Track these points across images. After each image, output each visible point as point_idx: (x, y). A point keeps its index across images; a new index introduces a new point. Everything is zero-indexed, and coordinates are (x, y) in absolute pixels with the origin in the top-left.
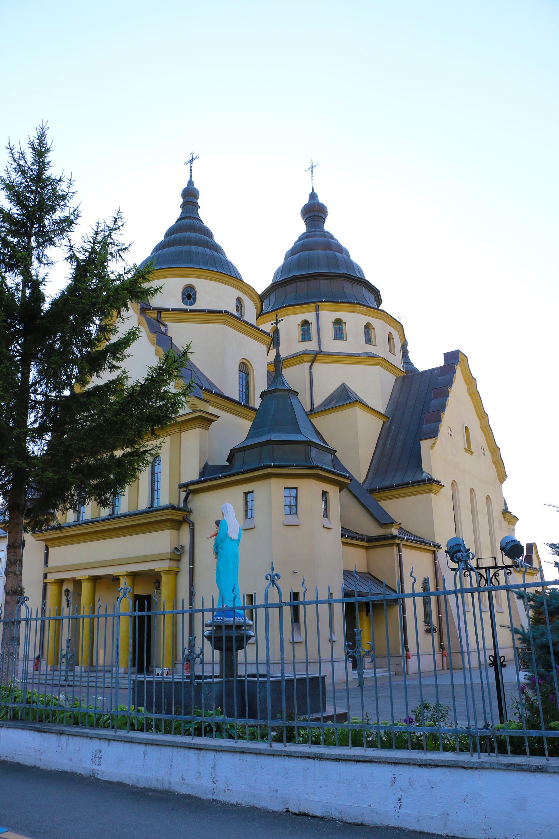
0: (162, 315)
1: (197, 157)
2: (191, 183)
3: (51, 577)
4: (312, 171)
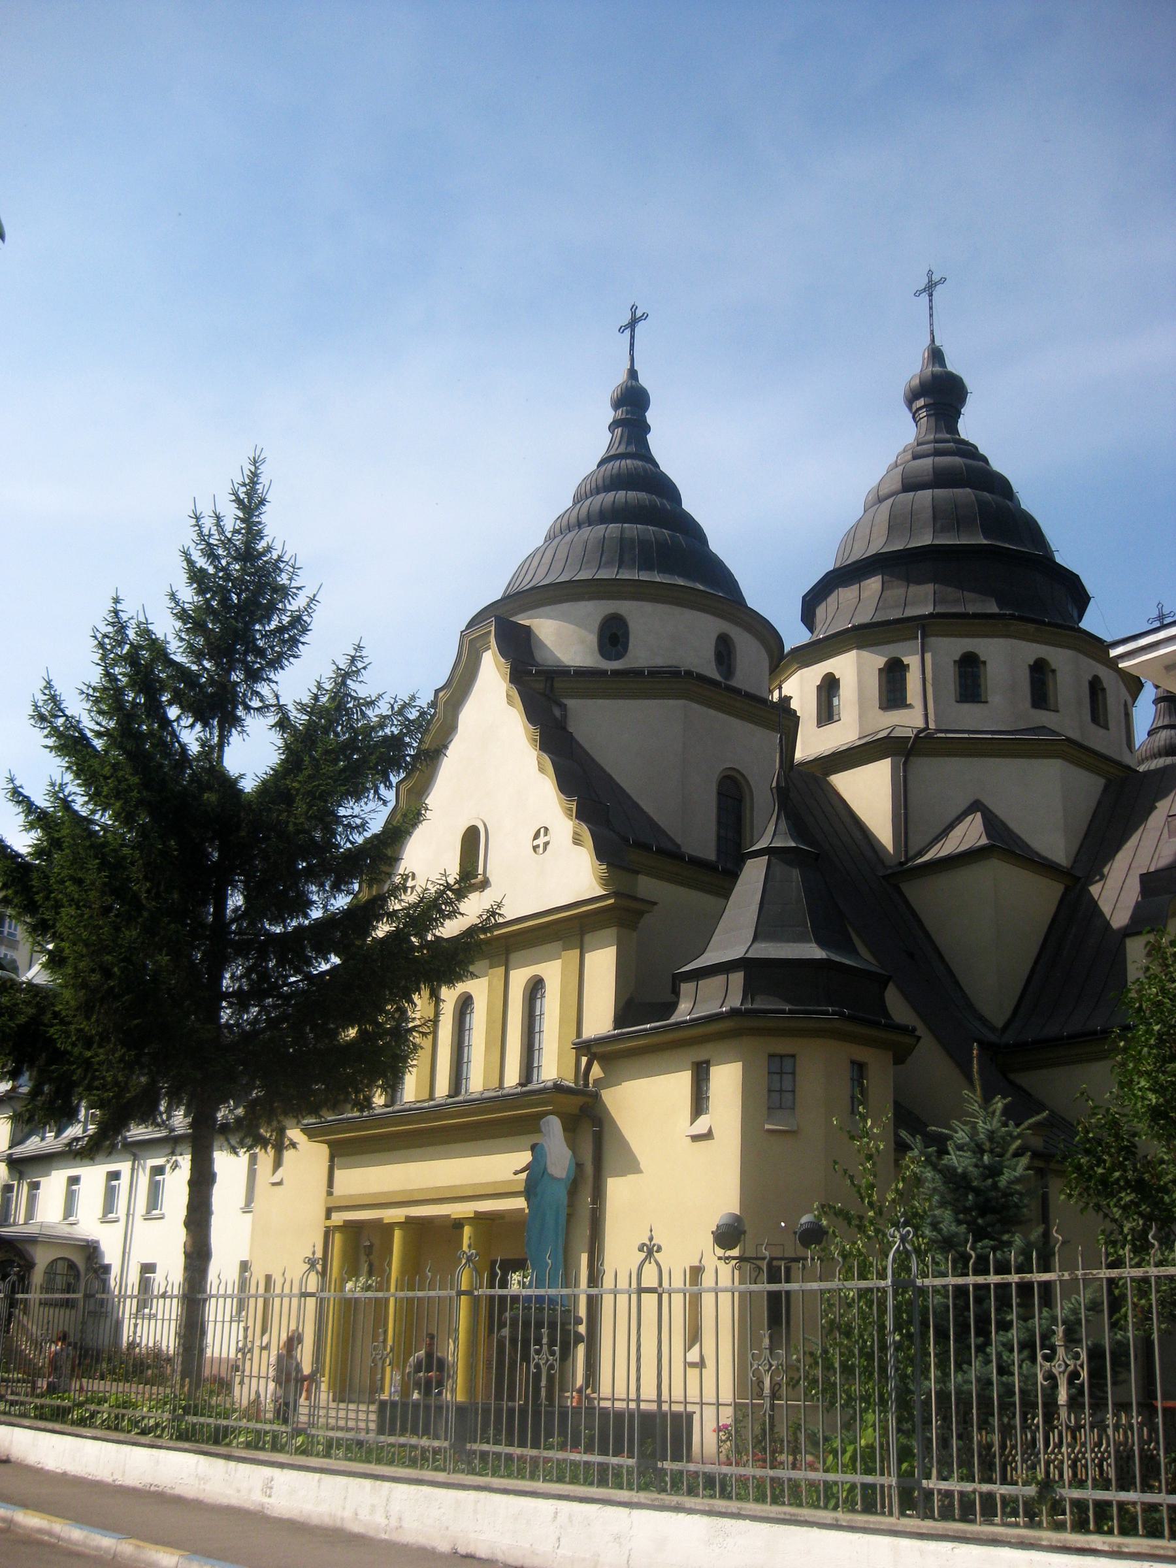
0: (556, 685)
1: (645, 316)
3: (338, 1218)
4: (931, 295)
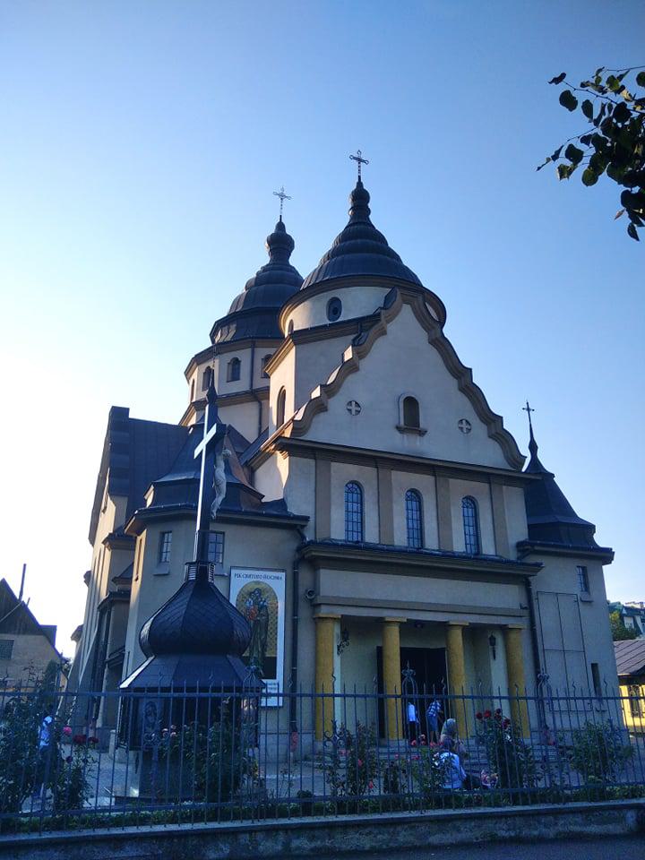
2: (360, 184)
